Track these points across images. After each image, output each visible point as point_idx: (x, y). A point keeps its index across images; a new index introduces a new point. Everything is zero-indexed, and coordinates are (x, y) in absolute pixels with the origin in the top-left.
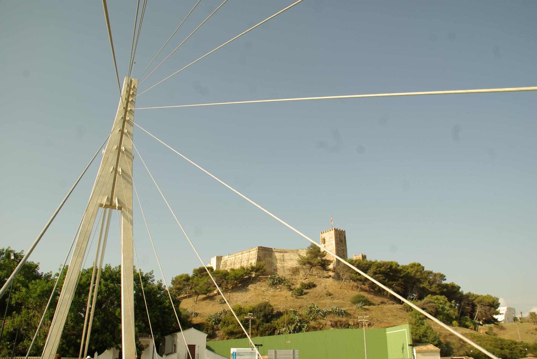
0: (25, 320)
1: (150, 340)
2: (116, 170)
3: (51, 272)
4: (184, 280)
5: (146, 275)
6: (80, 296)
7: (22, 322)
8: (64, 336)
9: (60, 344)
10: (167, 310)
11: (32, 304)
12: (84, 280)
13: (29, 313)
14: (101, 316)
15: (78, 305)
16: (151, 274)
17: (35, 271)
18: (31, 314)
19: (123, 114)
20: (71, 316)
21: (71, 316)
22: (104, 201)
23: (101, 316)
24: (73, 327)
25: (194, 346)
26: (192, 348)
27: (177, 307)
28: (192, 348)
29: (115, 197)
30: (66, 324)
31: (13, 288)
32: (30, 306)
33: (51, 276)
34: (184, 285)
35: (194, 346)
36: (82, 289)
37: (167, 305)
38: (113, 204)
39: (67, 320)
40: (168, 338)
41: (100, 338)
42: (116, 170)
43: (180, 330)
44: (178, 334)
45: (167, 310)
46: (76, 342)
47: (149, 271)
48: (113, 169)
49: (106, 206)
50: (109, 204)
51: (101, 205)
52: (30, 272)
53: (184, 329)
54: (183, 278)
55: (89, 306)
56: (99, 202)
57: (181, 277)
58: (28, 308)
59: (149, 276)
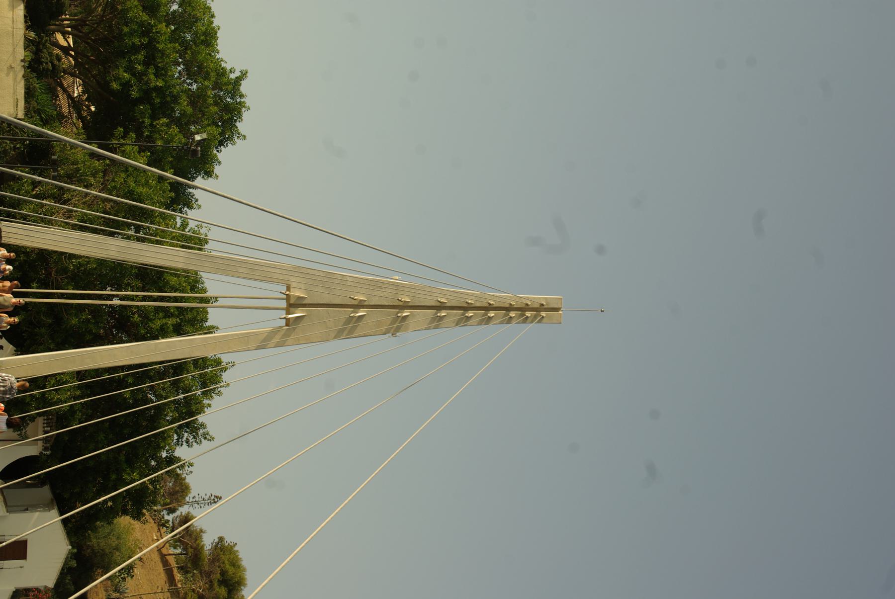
0: (78, 170)
1: (41, 429)
2: (360, 305)
3: (199, 207)
4: (223, 573)
5: (203, 426)
6: (137, 276)
7: (73, 164)
8: (44, 255)
9: (26, 248)
10: (114, 477)
11: (113, 180)
12: (173, 281)
13: (94, 175)
14: (91, 326)
15: (114, 273)
16: (205, 436)
17: (198, 172)
18: (92, 181)
19: (478, 305)
20: (88, 263)
21: (88, 263)
22: (296, 293)
23: (91, 326)
24: (65, 270)
25: (24, 557)
26: (18, 550)
27: (120, 507)
28: (18, 550)
29: (306, 311)
30: (72, 256)
31: (151, 132)
32: (110, 177)
33: (191, 208)
34: (209, 574)
35: (24, 557)
36: (151, 277)
37: (125, 476)
38: (292, 309)
39: (80, 257)
40: (46, 492)
41: (43, 330)
42: (360, 305)
43: (61, 514)
44: (54, 512)
45: (114, 477)
46: (33, 281)
47: (211, 429)
48: (361, 301)
49: (288, 297)
50: (292, 301)
51: (288, 289)
52: (199, 162)
53: (64, 522)
54: (231, 570)
55: (116, 302)
56: (293, 284)
57: (235, 563)
58: (105, 172)
59: (201, 432)
